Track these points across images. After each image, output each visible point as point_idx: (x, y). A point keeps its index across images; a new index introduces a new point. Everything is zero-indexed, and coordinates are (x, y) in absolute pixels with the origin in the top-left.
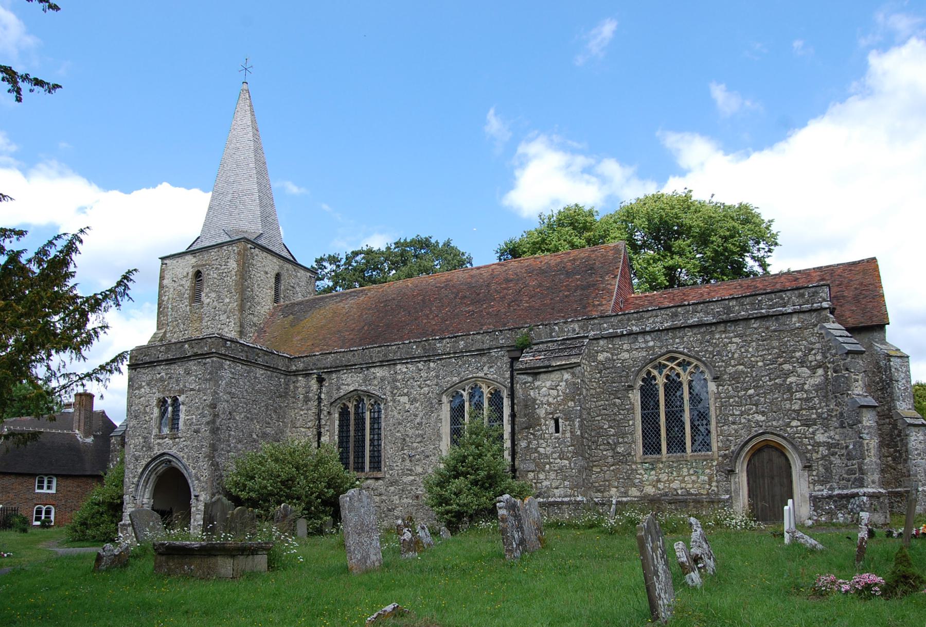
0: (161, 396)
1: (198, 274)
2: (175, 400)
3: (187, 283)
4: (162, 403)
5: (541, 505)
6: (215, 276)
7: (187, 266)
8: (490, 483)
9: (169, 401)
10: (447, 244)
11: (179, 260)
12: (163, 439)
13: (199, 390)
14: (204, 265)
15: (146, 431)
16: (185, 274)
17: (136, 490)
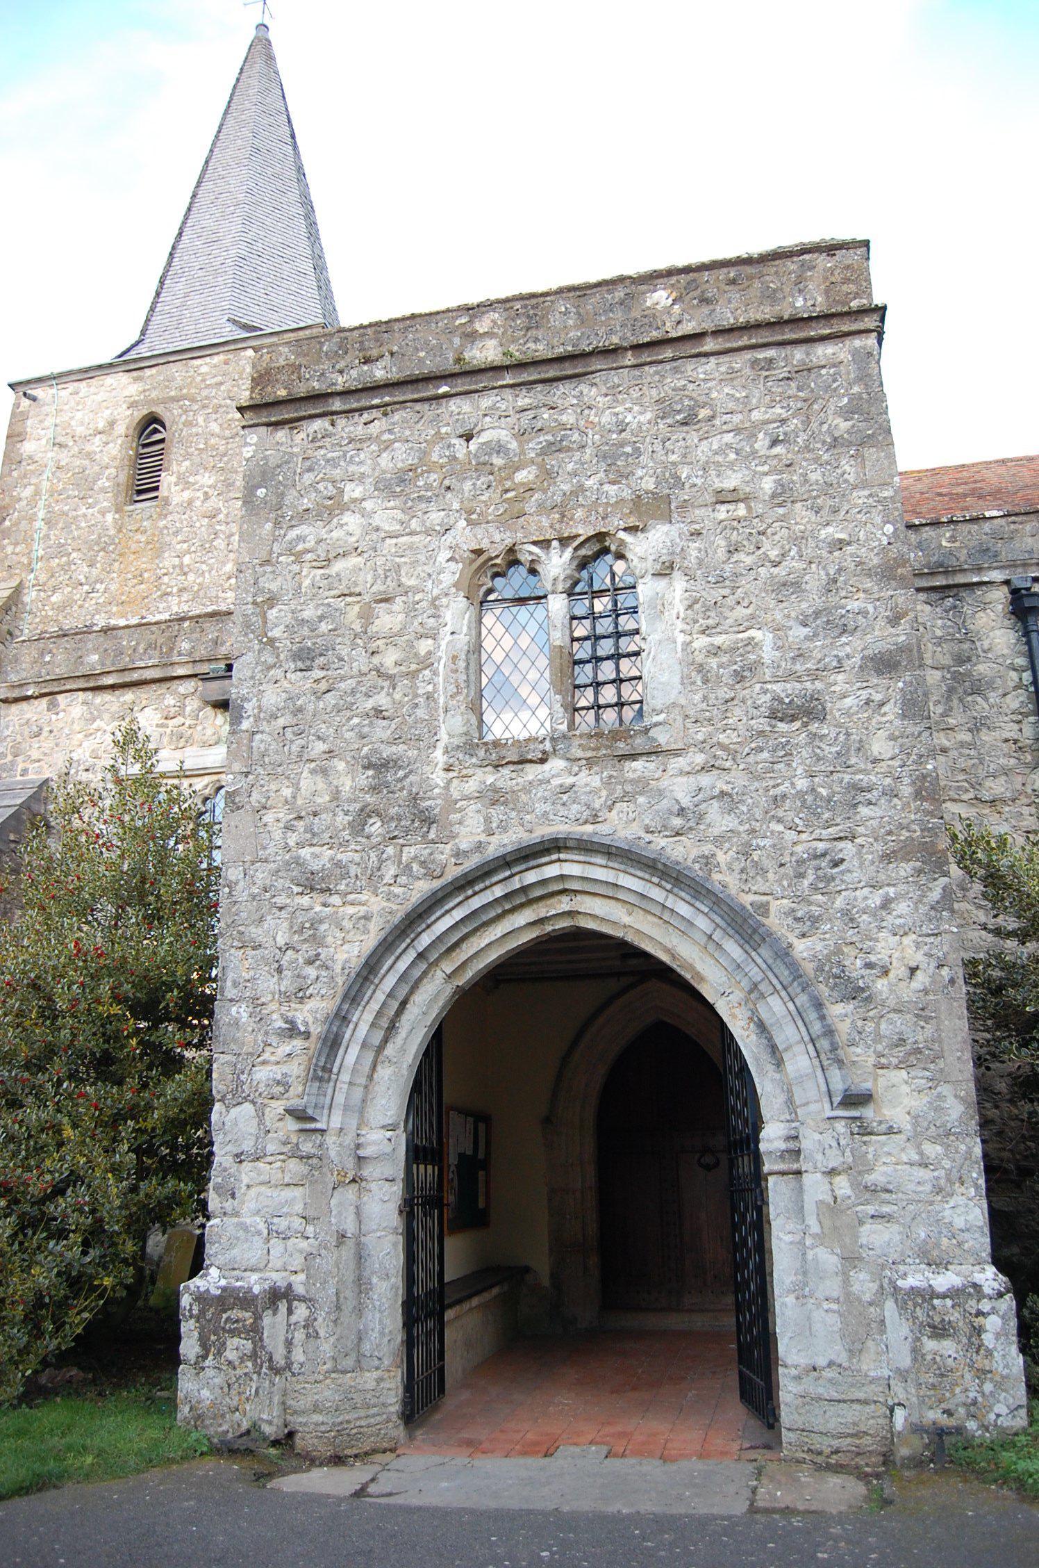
1: (150, 424)
3: (114, 452)
5: (313, 1119)
6: (215, 427)
7: (119, 399)
8: (316, 1078)
13: (782, 496)
17: (322, 1072)
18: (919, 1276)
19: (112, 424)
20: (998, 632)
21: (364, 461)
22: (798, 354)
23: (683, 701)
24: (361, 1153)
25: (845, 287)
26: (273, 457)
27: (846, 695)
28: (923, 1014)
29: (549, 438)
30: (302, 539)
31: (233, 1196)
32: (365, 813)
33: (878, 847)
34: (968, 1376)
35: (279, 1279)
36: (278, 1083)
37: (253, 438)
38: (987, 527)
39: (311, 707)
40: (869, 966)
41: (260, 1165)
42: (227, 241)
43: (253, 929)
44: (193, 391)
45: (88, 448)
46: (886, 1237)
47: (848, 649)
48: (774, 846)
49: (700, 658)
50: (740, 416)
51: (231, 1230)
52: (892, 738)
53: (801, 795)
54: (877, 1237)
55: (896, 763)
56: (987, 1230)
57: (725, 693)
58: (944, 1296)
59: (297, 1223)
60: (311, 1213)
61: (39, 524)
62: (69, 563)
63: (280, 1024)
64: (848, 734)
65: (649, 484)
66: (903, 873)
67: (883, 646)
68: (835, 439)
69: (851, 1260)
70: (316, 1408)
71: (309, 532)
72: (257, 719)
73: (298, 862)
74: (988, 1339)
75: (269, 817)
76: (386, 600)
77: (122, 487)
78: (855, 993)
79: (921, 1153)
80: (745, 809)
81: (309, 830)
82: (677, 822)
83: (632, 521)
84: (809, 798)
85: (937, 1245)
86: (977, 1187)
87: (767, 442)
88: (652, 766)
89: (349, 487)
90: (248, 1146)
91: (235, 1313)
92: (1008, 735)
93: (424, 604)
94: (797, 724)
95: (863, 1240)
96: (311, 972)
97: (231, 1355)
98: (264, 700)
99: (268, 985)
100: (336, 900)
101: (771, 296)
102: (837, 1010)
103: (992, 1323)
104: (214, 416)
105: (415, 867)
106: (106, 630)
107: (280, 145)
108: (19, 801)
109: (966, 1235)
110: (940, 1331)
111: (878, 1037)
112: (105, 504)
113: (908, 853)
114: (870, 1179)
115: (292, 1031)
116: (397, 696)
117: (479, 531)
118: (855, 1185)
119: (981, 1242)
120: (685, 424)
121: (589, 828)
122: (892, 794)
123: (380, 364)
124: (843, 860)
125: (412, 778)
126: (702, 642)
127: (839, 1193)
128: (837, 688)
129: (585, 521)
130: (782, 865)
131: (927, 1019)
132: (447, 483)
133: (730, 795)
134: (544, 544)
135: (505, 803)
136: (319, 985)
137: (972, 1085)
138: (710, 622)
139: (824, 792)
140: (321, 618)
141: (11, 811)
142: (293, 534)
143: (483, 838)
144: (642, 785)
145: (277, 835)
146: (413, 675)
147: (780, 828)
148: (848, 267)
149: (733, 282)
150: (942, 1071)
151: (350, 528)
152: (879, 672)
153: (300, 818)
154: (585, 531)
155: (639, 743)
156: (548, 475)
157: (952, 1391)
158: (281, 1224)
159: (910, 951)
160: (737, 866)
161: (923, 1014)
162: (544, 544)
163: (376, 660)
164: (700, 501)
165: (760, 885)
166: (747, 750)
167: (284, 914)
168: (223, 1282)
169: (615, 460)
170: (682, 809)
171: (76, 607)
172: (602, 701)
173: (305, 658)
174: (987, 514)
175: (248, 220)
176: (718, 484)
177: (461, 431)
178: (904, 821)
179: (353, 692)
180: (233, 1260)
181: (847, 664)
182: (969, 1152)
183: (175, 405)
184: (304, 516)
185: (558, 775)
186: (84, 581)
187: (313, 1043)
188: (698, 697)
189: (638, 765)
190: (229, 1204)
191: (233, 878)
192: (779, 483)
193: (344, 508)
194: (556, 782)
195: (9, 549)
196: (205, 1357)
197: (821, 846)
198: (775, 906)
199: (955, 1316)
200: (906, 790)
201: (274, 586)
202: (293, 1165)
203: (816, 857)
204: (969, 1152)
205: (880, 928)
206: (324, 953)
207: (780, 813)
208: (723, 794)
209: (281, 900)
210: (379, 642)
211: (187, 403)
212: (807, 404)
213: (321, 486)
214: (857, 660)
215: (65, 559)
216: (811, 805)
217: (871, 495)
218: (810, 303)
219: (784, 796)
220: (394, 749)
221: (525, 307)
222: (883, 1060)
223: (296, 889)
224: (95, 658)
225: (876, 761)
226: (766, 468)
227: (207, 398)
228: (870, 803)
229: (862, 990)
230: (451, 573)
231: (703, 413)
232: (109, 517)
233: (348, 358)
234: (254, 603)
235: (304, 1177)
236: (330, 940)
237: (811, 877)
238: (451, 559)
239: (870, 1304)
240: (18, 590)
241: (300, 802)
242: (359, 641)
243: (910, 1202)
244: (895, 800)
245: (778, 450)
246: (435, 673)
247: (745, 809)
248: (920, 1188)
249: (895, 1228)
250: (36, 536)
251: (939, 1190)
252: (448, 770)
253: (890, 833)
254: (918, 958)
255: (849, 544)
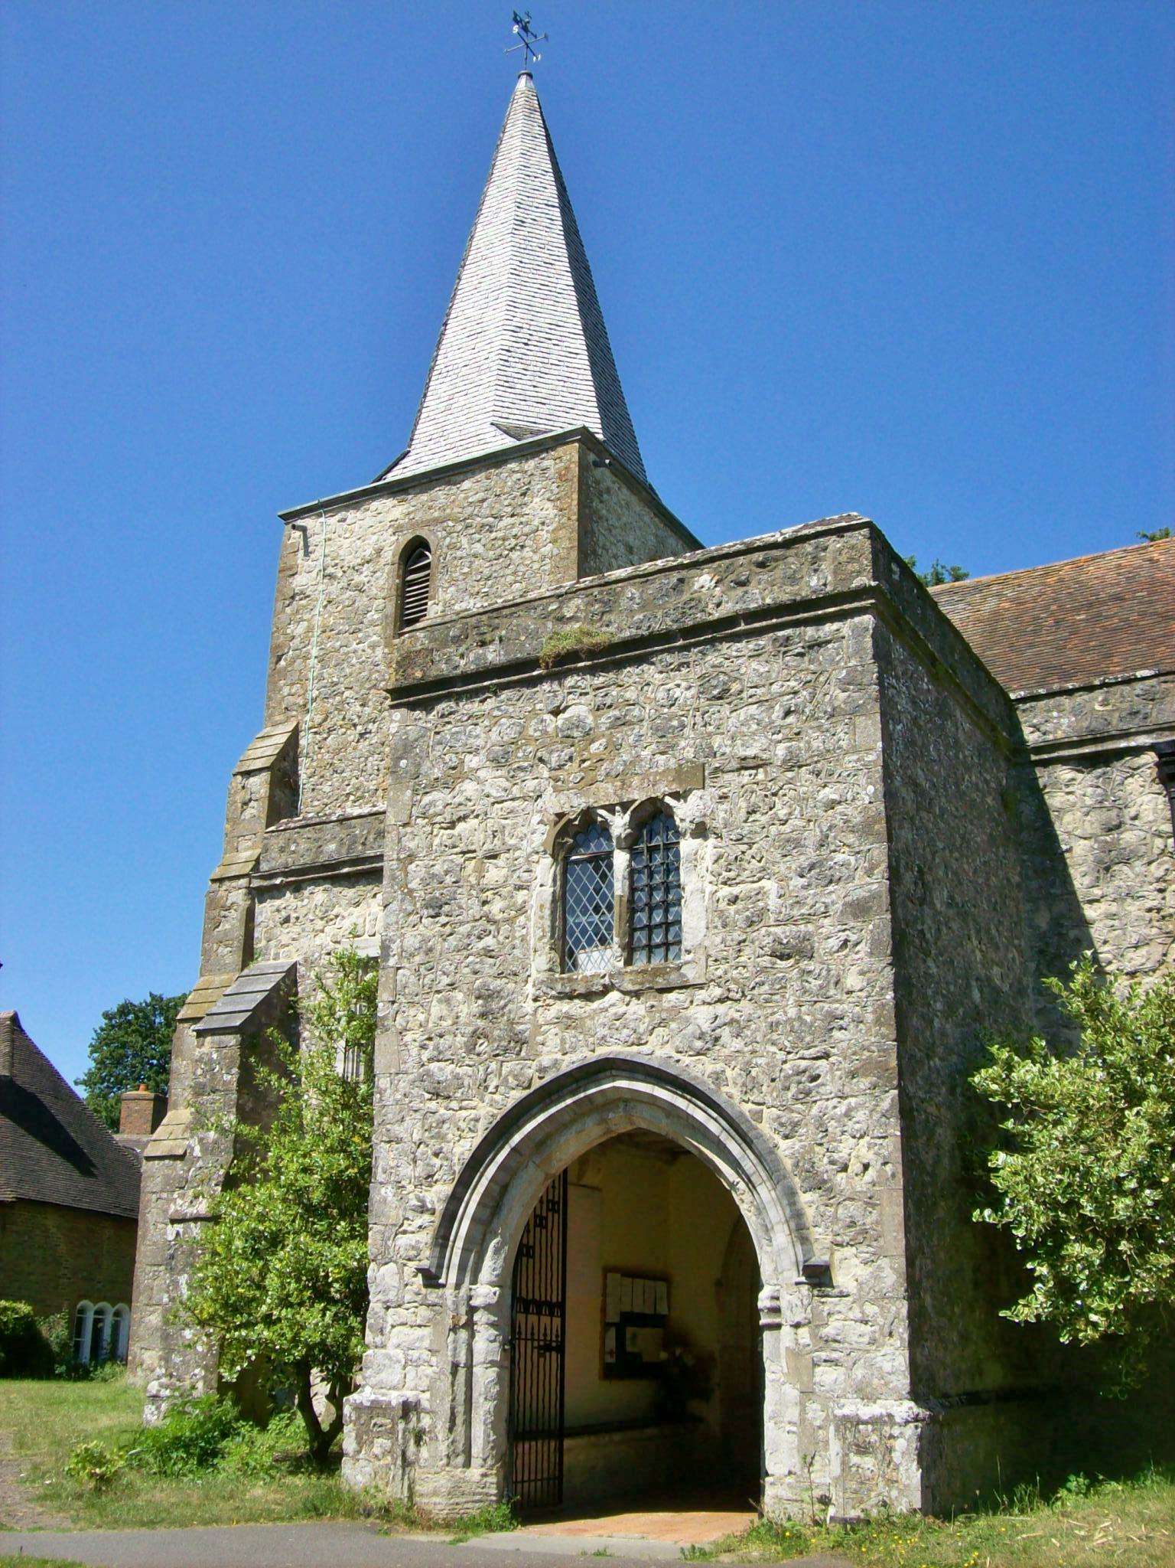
0: (574, 803)
1: (414, 553)
2: (653, 820)
3: (382, 580)
4: (577, 835)
6: (478, 548)
9: (619, 824)
10: (106, 1015)
11: (351, 515)
12: (589, 996)
13: (793, 763)
14: (437, 521)
15: (488, 966)
16: (369, 552)
18: (853, 1408)
19: (379, 552)
20: (1146, 798)
21: (479, 736)
22: (810, 632)
23: (707, 943)
24: (473, 1303)
25: (849, 567)
26: (413, 732)
27: (828, 935)
28: (870, 1202)
29: (617, 713)
30: (432, 804)
31: (382, 1332)
32: (476, 1035)
33: (846, 1065)
34: (881, 1484)
35: (410, 1395)
36: (413, 1248)
37: (397, 715)
38: (1139, 687)
39: (439, 947)
40: (832, 1163)
41: (399, 1310)
42: (491, 333)
43: (396, 1127)
44: (456, 510)
45: (358, 579)
46: (834, 1375)
47: (834, 896)
48: (767, 1064)
49: (723, 905)
50: (763, 690)
51: (380, 1360)
52: (862, 973)
53: (790, 1020)
54: (826, 1376)
55: (863, 994)
56: (907, 1373)
57: (737, 936)
58: (866, 1423)
59: (426, 1355)
60: (435, 1347)
61: (312, 662)
62: (342, 702)
63: (414, 1202)
64: (829, 971)
65: (689, 753)
66: (862, 1086)
67: (862, 893)
68: (834, 709)
69: (807, 1393)
70: (435, 1493)
71: (439, 797)
72: (401, 956)
73: (428, 1073)
74: (896, 1456)
75: (408, 1037)
76: (495, 857)
77: (391, 620)
78: (818, 1184)
79: (863, 1312)
80: (749, 1033)
81: (436, 1048)
82: (698, 1044)
83: (675, 787)
84: (796, 1024)
85: (869, 1384)
86: (902, 1339)
87: (781, 714)
88: (682, 997)
89: (469, 757)
90: (392, 1296)
91: (379, 1420)
92: (1149, 904)
93: (521, 860)
94: (792, 961)
95: (817, 1379)
96: (437, 1162)
97: (377, 1450)
98: (406, 943)
99: (407, 1170)
100: (454, 1105)
101: (793, 579)
102: (804, 1198)
103: (900, 1444)
104: (477, 536)
105: (510, 1079)
106: (343, 820)
107: (546, 210)
108: (269, 987)
109: (893, 1377)
110: (863, 1449)
111: (836, 1219)
112: (375, 638)
113: (866, 1070)
114: (825, 1331)
115: (422, 1209)
116: (501, 938)
117: (563, 797)
118: (814, 1335)
119: (903, 1382)
120: (721, 698)
121: (635, 1048)
122: (859, 1021)
123: (492, 648)
124: (819, 1076)
125: (510, 1006)
126: (725, 891)
127: (801, 1341)
128: (823, 930)
129: (641, 788)
130: (773, 1080)
131: (874, 1206)
132: (539, 754)
133: (738, 1022)
134: (610, 809)
135: (575, 1028)
136: (441, 1173)
137: (904, 1259)
138: (732, 874)
139: (808, 1019)
140: (447, 872)
141: (260, 997)
142: (427, 799)
143: (559, 1056)
144: (675, 1011)
145: (414, 1051)
146: (510, 921)
147: (774, 1049)
148: (853, 547)
149: (762, 565)
150: (881, 1247)
151: (468, 794)
152: (855, 917)
153: (430, 1039)
154: (639, 796)
155: (674, 979)
156: (614, 747)
157: (869, 1496)
158: (414, 1354)
159: (864, 1151)
160: (740, 1081)
161: (870, 1202)
162: (610, 809)
163: (486, 908)
164: (728, 768)
165: (755, 1097)
166: (753, 984)
167: (418, 1115)
168: (373, 1397)
169: (666, 735)
170: (703, 1033)
171: (350, 749)
172: (653, 943)
173: (436, 907)
174: (1139, 674)
175: (513, 305)
176: (743, 752)
177: (550, 708)
178: (866, 1043)
179: (469, 936)
180: (381, 1381)
181: (832, 910)
182: (898, 1313)
183: (439, 527)
184: (435, 784)
185: (613, 1005)
186: (356, 721)
187: (437, 1219)
188: (718, 940)
189: (672, 996)
190: (379, 1339)
191: (382, 1086)
192: (789, 750)
193: (462, 777)
194: (612, 1010)
195: (286, 690)
196: (359, 1452)
197: (804, 1064)
198: (767, 1113)
199: (874, 1438)
200: (870, 1017)
201: (412, 845)
202: (424, 1312)
203: (798, 1074)
204: (898, 1313)
205: (843, 1133)
206: (446, 1147)
207: (775, 1036)
208: (732, 1021)
209: (415, 1105)
210: (489, 893)
211: (450, 523)
212: (814, 677)
213: (447, 758)
214: (839, 906)
215: (338, 698)
216: (797, 1028)
217: (858, 760)
218: (822, 582)
219: (778, 1023)
220: (498, 982)
221: (601, 593)
222: (839, 1239)
223: (428, 1096)
224: (332, 846)
225: (849, 992)
226: (780, 737)
227: (470, 516)
228: (841, 1028)
229: (825, 1182)
230: (541, 835)
231: (735, 687)
232: (379, 652)
233: (469, 641)
234: (398, 859)
235: (430, 1320)
236: (450, 1136)
237: (793, 1089)
238: (541, 822)
239: (820, 1428)
240: (295, 734)
241: (430, 1025)
242: (474, 893)
243: (853, 1350)
244: (861, 1026)
245: (791, 719)
246: (528, 919)
247: (749, 1033)
248: (861, 1340)
249: (842, 1369)
250: (310, 676)
251: (873, 1342)
252: (535, 1000)
253: (854, 1054)
254: (869, 1156)
255: (839, 803)
